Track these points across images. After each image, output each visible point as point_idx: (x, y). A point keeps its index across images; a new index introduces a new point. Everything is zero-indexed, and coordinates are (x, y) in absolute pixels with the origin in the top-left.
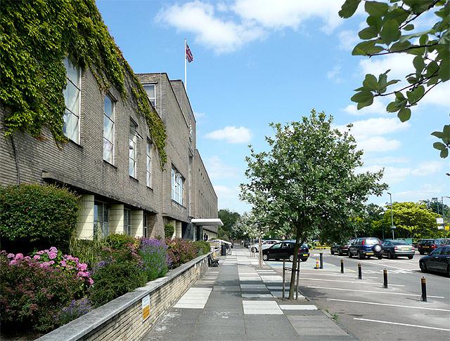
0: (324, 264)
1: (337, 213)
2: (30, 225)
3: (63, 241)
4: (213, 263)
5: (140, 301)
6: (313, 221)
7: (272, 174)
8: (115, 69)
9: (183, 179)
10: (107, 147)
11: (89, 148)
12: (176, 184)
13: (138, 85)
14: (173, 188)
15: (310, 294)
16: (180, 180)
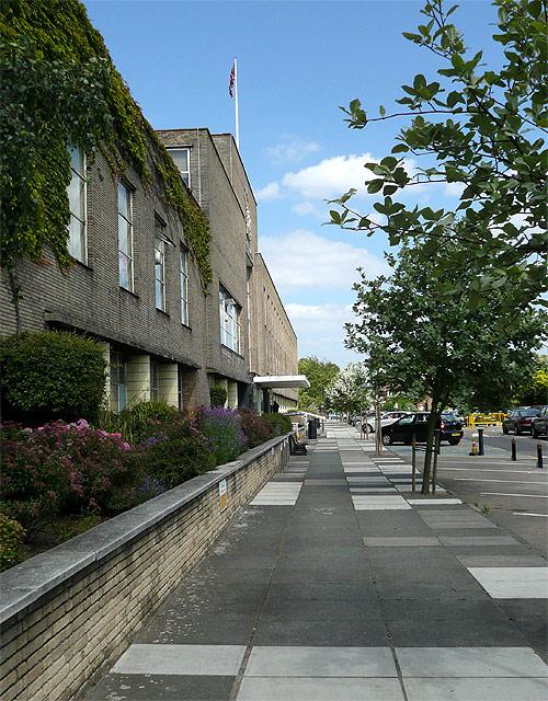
0: (485, 448)
1: (495, 367)
2: (51, 389)
3: (92, 413)
4: (298, 450)
5: (218, 484)
6: (458, 378)
7: (394, 310)
8: (133, 140)
9: (239, 308)
10: (123, 265)
11: (100, 270)
12: (227, 317)
13: (159, 149)
14: (223, 324)
15: (453, 488)
16: (233, 311)
